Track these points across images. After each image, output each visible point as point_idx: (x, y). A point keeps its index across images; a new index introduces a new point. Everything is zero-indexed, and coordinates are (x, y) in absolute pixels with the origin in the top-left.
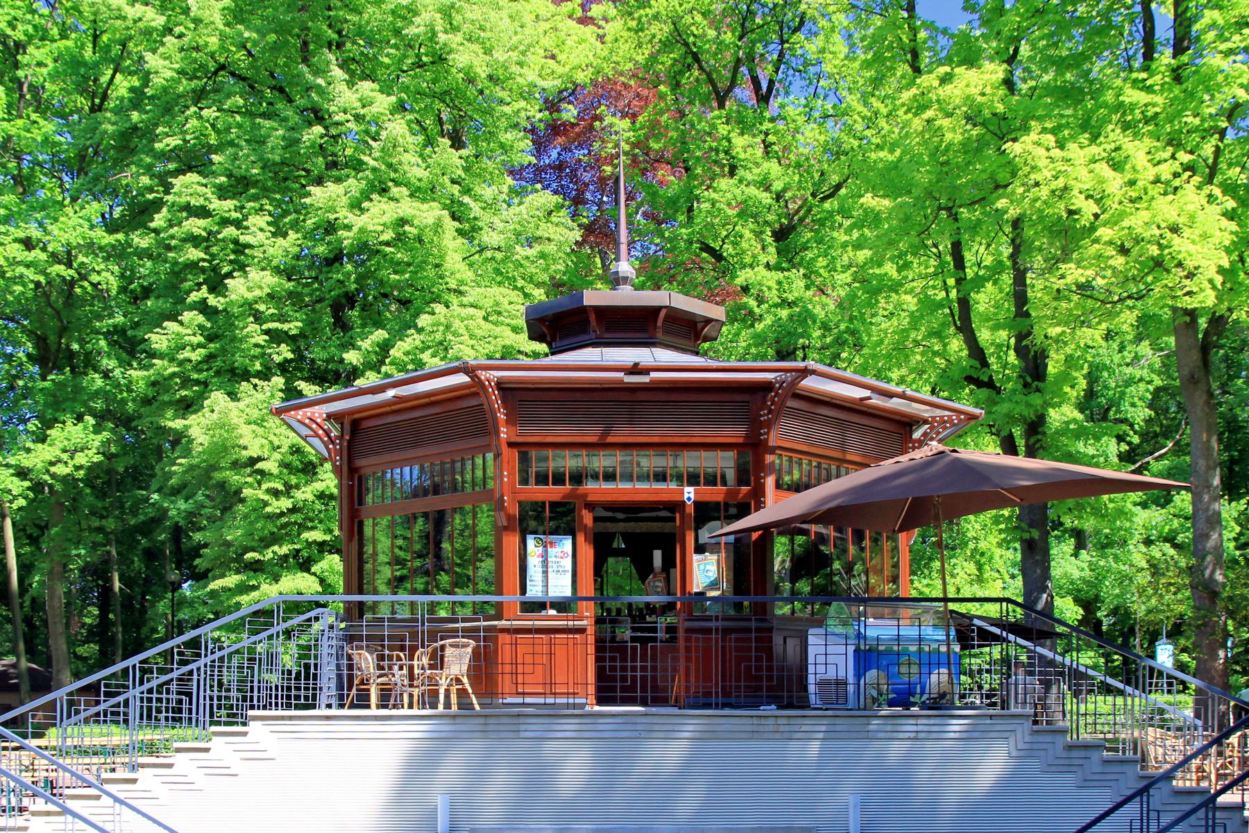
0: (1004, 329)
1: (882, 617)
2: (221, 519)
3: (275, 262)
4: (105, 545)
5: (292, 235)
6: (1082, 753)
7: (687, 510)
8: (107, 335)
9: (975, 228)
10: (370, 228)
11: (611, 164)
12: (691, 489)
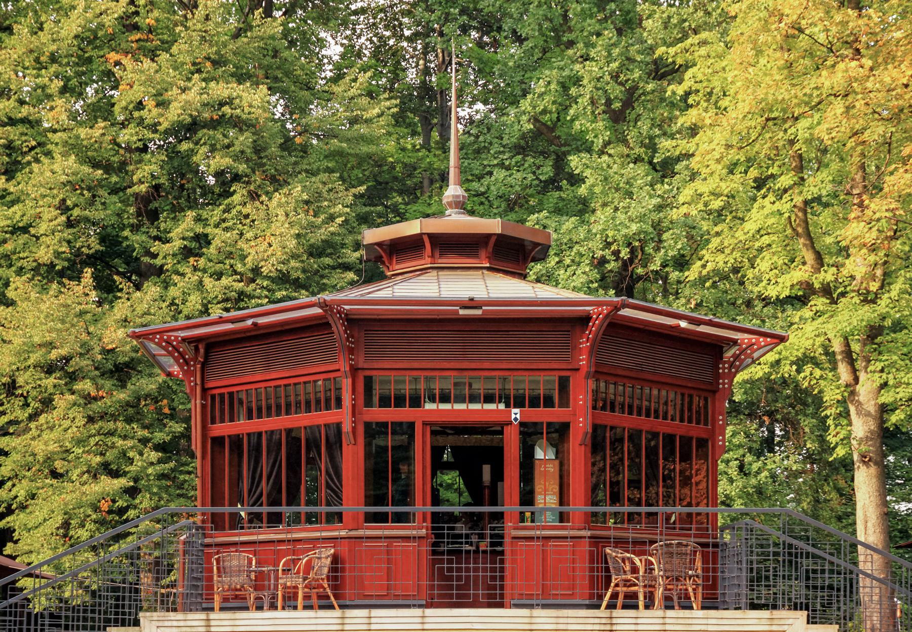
12: (517, 410)
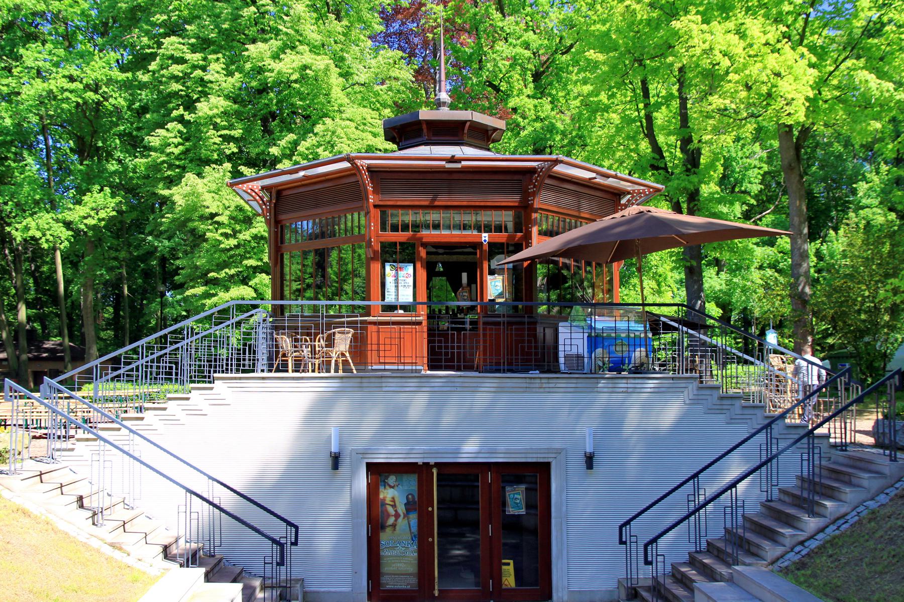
0: (674, 135)
1: (603, 316)
2: (192, 253)
3: (226, 93)
4: (119, 268)
5: (237, 75)
6: (729, 402)
7: (484, 248)
8: (120, 135)
9: (655, 71)
10: (284, 70)
11: (432, 32)
12: (486, 235)
